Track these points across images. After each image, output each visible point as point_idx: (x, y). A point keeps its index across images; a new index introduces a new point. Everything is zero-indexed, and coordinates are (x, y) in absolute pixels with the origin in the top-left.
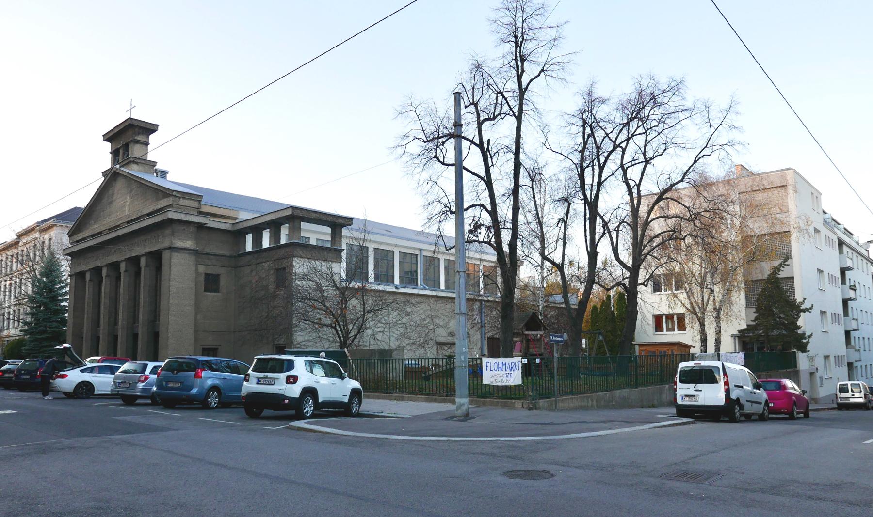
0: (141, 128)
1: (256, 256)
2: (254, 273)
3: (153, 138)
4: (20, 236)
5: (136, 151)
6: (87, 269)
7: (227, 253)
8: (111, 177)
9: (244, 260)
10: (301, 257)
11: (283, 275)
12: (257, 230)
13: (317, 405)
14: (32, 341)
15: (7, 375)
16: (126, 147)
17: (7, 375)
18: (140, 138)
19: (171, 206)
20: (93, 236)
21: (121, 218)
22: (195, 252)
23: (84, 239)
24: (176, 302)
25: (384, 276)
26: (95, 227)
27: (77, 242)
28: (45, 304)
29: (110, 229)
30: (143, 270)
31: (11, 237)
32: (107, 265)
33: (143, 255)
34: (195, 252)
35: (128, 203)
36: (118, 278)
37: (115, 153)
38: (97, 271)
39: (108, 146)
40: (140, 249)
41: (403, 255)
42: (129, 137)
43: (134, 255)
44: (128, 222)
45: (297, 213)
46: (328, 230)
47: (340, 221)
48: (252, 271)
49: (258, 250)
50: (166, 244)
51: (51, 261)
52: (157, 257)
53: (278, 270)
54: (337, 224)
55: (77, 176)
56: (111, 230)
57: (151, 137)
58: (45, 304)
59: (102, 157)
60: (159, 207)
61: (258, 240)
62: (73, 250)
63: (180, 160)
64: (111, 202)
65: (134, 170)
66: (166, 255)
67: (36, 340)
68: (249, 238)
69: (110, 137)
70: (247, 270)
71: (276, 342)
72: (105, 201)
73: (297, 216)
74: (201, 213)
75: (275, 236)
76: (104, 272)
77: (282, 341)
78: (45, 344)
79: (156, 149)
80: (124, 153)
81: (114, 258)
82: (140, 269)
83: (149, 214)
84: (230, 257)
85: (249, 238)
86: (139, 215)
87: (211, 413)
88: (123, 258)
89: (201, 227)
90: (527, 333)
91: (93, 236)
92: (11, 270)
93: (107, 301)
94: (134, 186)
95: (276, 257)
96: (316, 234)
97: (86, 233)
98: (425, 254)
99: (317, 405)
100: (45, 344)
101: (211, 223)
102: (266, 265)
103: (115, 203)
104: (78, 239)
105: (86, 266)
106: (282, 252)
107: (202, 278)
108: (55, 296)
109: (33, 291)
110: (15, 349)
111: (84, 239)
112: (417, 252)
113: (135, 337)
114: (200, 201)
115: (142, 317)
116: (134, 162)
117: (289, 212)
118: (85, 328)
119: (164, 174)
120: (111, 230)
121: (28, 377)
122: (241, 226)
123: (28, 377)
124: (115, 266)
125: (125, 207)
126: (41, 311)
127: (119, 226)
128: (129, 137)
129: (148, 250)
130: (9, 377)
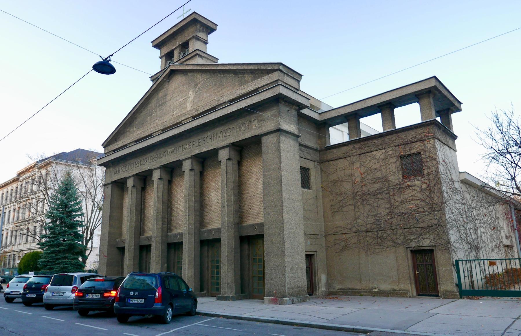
1: (357, 146)
3: (211, 37)
4: (19, 175)
5: (194, 46)
7: (315, 146)
9: (331, 155)
12: (352, 117)
13: (95, 290)
14: (49, 253)
15: (90, 296)
16: (185, 46)
17: (90, 296)
18: (201, 35)
20: (137, 141)
21: (184, 114)
27: (114, 151)
28: (61, 219)
29: (162, 130)
31: (14, 175)
32: (133, 176)
35: (191, 99)
37: (169, 56)
39: (157, 52)
50: (269, 126)
51: (67, 180)
56: (164, 130)
58: (61, 219)
60: (252, 88)
67: (53, 252)
69: (158, 44)
70: (343, 163)
71: (412, 244)
77: (426, 243)
78: (61, 256)
83: (272, 83)
84: (316, 150)
90: (93, 260)
92: (26, 193)
97: (120, 144)
99: (95, 290)
100: (61, 256)
103: (168, 104)
108: (70, 212)
109: (50, 207)
110: (30, 263)
121: (140, 301)
123: (140, 301)
126: (57, 226)
127: (180, 122)
128: (183, 40)
130: (92, 300)
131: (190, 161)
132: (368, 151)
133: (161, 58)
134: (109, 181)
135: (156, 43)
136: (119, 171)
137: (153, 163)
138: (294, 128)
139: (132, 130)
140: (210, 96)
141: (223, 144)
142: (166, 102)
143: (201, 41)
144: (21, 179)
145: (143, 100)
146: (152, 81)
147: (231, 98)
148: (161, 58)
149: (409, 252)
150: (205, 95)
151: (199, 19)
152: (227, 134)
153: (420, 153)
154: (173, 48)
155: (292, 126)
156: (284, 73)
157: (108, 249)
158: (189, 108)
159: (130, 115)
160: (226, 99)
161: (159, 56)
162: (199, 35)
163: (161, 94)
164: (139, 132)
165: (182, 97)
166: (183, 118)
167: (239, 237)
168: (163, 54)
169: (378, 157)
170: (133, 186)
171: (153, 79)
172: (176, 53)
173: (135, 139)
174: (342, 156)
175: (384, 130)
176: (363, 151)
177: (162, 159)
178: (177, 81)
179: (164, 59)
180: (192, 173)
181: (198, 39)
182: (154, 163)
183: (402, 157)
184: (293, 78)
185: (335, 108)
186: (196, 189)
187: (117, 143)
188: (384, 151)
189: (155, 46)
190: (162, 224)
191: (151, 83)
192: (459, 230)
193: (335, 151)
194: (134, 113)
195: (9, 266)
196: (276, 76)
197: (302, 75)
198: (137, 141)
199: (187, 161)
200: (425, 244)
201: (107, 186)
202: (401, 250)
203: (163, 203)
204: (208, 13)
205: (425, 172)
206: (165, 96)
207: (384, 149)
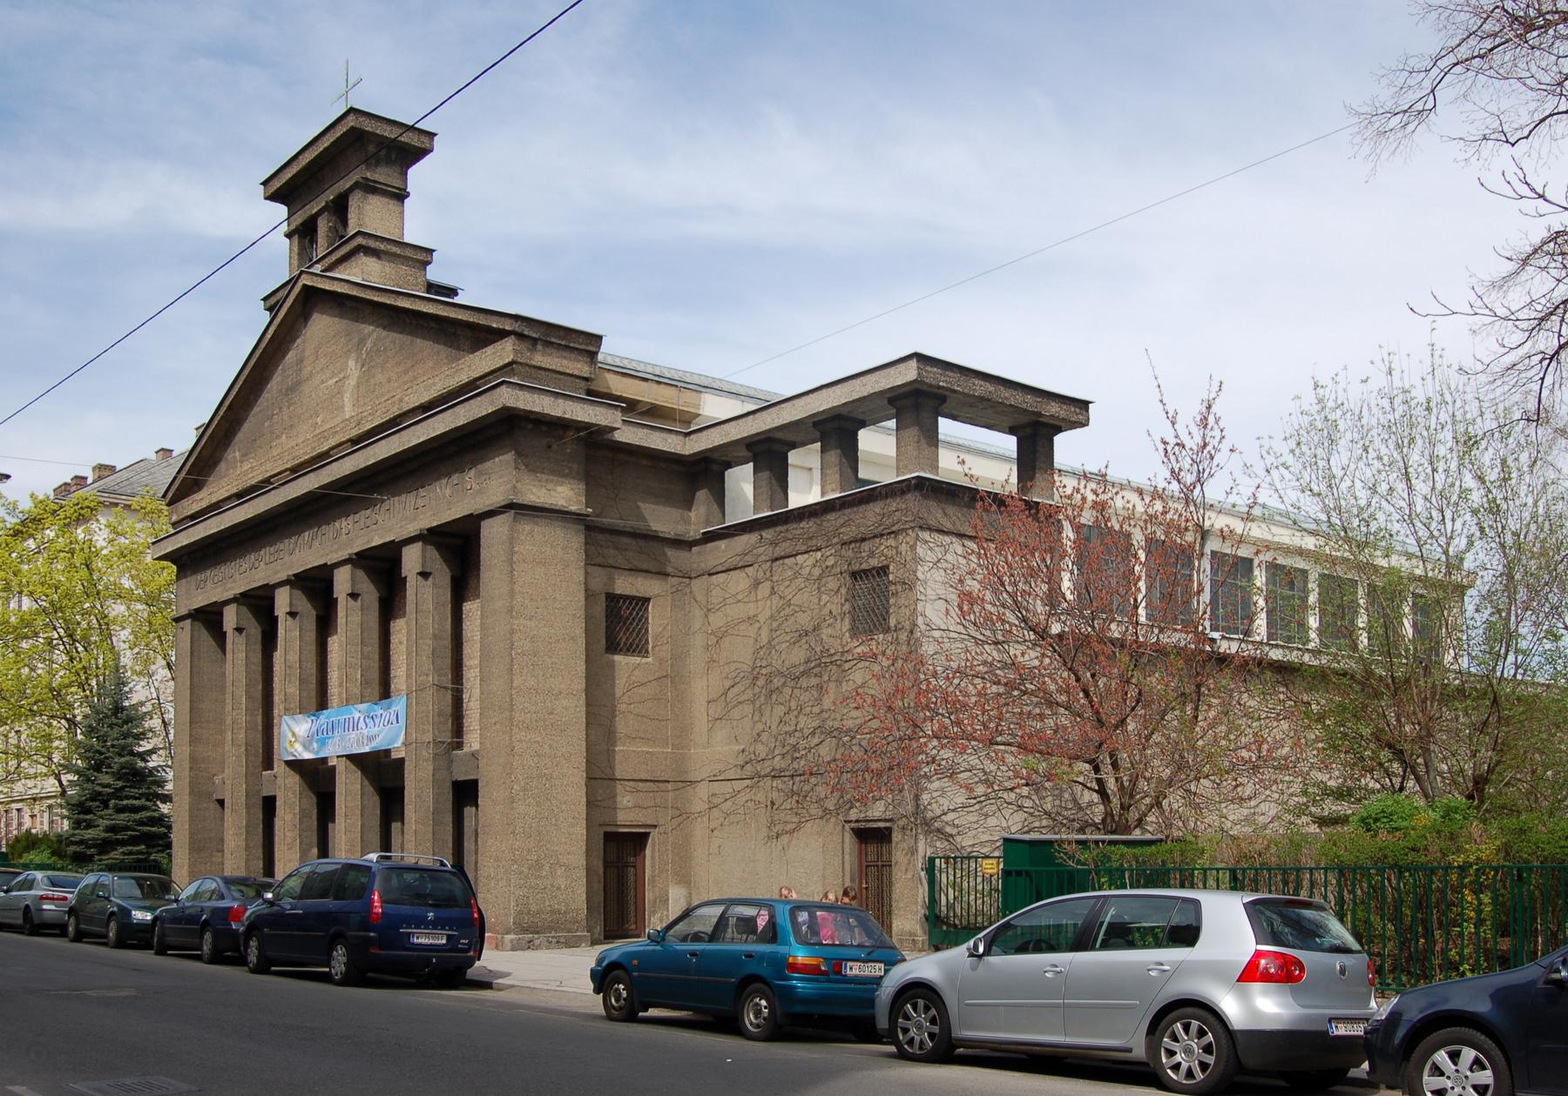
0: (382, 142)
1: (768, 534)
2: (765, 589)
3: (418, 175)
5: (368, 215)
8: (295, 308)
12: (769, 453)
16: (339, 208)
18: (382, 175)
19: (508, 367)
23: (215, 508)
24: (532, 682)
25: (1173, 604)
27: (192, 517)
29: (293, 470)
35: (352, 382)
37: (304, 233)
38: (259, 603)
42: (347, 169)
43: (377, 541)
45: (934, 376)
46: (1008, 444)
47: (1053, 409)
52: (458, 546)
54: (1037, 421)
56: (298, 471)
57: (414, 173)
60: (464, 378)
62: (184, 540)
64: (294, 388)
65: (364, 273)
66: (493, 532)
73: (927, 394)
74: (597, 395)
77: (877, 810)
80: (333, 230)
82: (274, 621)
83: (425, 408)
86: (395, 411)
88: (343, 555)
89: (594, 441)
95: (849, 532)
96: (978, 454)
104: (196, 507)
106: (870, 516)
111: (215, 508)
114: (592, 355)
117: (909, 373)
120: (298, 471)
125: (350, 393)
127: (326, 454)
128: (347, 169)
131: (348, 568)
132: (789, 551)
133: (289, 235)
135: (277, 184)
137: (333, 544)
138: (570, 493)
140: (389, 381)
141: (412, 529)
142: (299, 383)
143: (384, 193)
145: (246, 372)
146: (270, 309)
147: (425, 397)
148: (289, 235)
149: (848, 837)
150: (380, 377)
151: (368, 126)
152: (420, 503)
153: (887, 567)
155: (560, 489)
156: (535, 341)
158: (349, 411)
159: (221, 413)
160: (414, 400)
162: (376, 177)
163: (291, 356)
164: (246, 466)
165: (334, 375)
166: (332, 442)
167: (449, 784)
168: (293, 227)
169: (805, 572)
171: (272, 303)
172: (323, 226)
173: (235, 490)
174: (736, 561)
175: (823, 494)
176: (779, 552)
177: (294, 558)
178: (321, 325)
179: (296, 239)
180: (242, 639)
181: (370, 188)
182: (277, 565)
183: (855, 575)
184: (567, 347)
186: (367, 649)
187: (197, 496)
188: (819, 554)
189: (272, 197)
194: (230, 407)
195: (140, 853)
196: (501, 353)
197: (600, 338)
198: (243, 495)
199: (342, 569)
200: (877, 814)
201: (181, 624)
202: (832, 825)
204: (395, 103)
205: (892, 622)
206: (300, 361)
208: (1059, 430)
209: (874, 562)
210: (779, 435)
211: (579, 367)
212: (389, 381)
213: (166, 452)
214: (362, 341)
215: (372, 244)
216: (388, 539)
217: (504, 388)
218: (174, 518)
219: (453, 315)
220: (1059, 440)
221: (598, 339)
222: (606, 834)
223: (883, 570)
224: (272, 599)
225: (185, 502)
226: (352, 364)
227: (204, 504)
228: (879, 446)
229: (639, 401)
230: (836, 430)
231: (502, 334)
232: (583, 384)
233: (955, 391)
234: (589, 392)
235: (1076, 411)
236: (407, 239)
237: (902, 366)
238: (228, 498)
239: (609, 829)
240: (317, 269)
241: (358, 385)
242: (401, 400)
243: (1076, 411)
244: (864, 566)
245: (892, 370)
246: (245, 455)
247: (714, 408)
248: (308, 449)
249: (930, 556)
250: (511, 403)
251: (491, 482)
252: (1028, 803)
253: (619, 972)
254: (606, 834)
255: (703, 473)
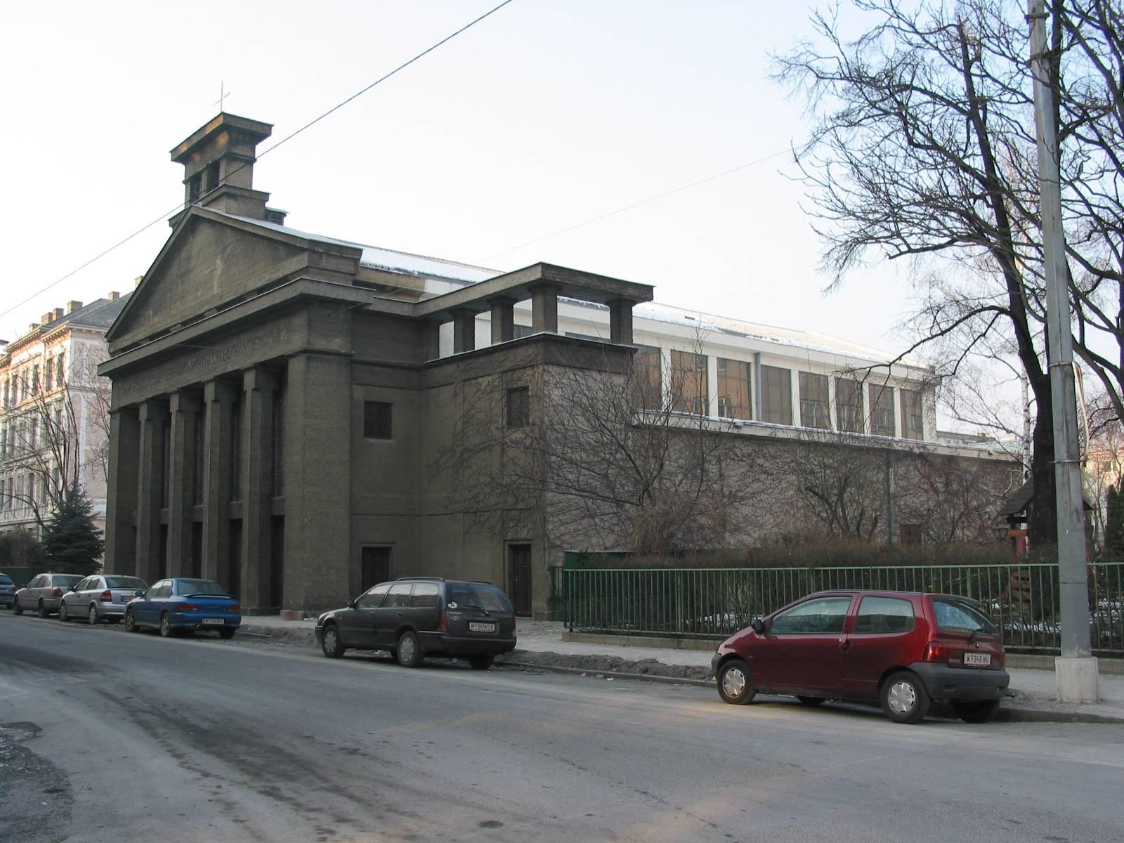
1: (462, 365)
2: (459, 399)
6: (143, 399)
8: (186, 227)
10: (559, 365)
11: (517, 401)
12: (463, 315)
16: (214, 168)
19: (305, 270)
22: (351, 361)
26: (154, 322)
27: (124, 350)
29: (184, 324)
30: (249, 396)
32: (148, 401)
33: (249, 369)
34: (351, 361)
35: (219, 272)
36: (167, 423)
37: (192, 182)
38: (160, 403)
39: (180, 169)
40: (244, 356)
41: (723, 362)
42: (218, 154)
43: (230, 369)
44: (219, 308)
45: (550, 275)
47: (631, 291)
48: (455, 395)
49: (468, 355)
52: (275, 372)
53: (510, 392)
54: (622, 297)
55: (117, 234)
59: (169, 191)
60: (280, 275)
61: (465, 334)
62: (117, 364)
63: (305, 191)
66: (296, 368)
68: (447, 331)
69: (182, 155)
71: (510, 536)
72: (174, 270)
73: (551, 283)
75: (504, 322)
76: (174, 404)
77: (524, 533)
79: (270, 172)
81: (190, 378)
82: (170, 415)
83: (260, 290)
85: (447, 331)
86: (241, 292)
87: (90, 626)
88: (210, 377)
89: (358, 310)
91: (151, 338)
93: (180, 458)
94: (230, 237)
95: (508, 365)
96: (583, 319)
98: (763, 361)
101: (378, 304)
102: (484, 382)
104: (125, 344)
105: (142, 391)
106: (522, 353)
107: (360, 412)
112: (750, 359)
113: (236, 525)
115: (247, 484)
116: (230, 196)
117: (537, 275)
118: (140, 509)
119: (278, 217)
120: (186, 324)
122: (431, 308)
124: (194, 393)
125: (214, 281)
127: (201, 316)
128: (218, 154)
129: (259, 358)
133: (184, 182)
134: (116, 408)
136: (129, 389)
137: (204, 370)
139: (147, 313)
141: (249, 362)
142: (188, 272)
144: (15, 361)
147: (260, 284)
148: (184, 182)
154: (200, 170)
155: (336, 340)
157: (883, 616)
158: (216, 291)
161: (183, 179)
163: (184, 254)
164: (156, 320)
170: (256, 390)
171: (174, 222)
173: (148, 335)
176: (467, 376)
185: (442, 294)
190: (184, 490)
191: (170, 231)
192: (496, 504)
193: (437, 372)
196: (301, 261)
200: (523, 536)
203: (185, 453)
206: (189, 258)
207: (490, 375)
208: (635, 303)
209: (520, 384)
210: (467, 306)
211: (348, 267)
212: (239, 273)
213: (116, 294)
214: (225, 248)
215: (232, 191)
216: (237, 368)
217: (301, 282)
218: (112, 350)
219: (275, 238)
220: (634, 308)
221: (359, 252)
222: (364, 548)
223: (526, 388)
224: (169, 401)
225: (119, 341)
226: (218, 261)
227: (129, 343)
228: (524, 312)
229: (386, 286)
230: (500, 300)
231: (303, 250)
232: (350, 277)
233: (567, 284)
234: (356, 283)
235: (645, 293)
236: (254, 189)
237: (533, 270)
238: (145, 339)
239: (365, 545)
240: (200, 205)
241: (222, 274)
242: (245, 286)
243: (645, 293)
244: (515, 386)
245: (528, 273)
246: (155, 313)
247: (434, 288)
248: (195, 312)
249: (552, 381)
250: (306, 291)
251: (290, 339)
252: (617, 528)
253: (332, 626)
254: (364, 548)
255: (426, 325)
